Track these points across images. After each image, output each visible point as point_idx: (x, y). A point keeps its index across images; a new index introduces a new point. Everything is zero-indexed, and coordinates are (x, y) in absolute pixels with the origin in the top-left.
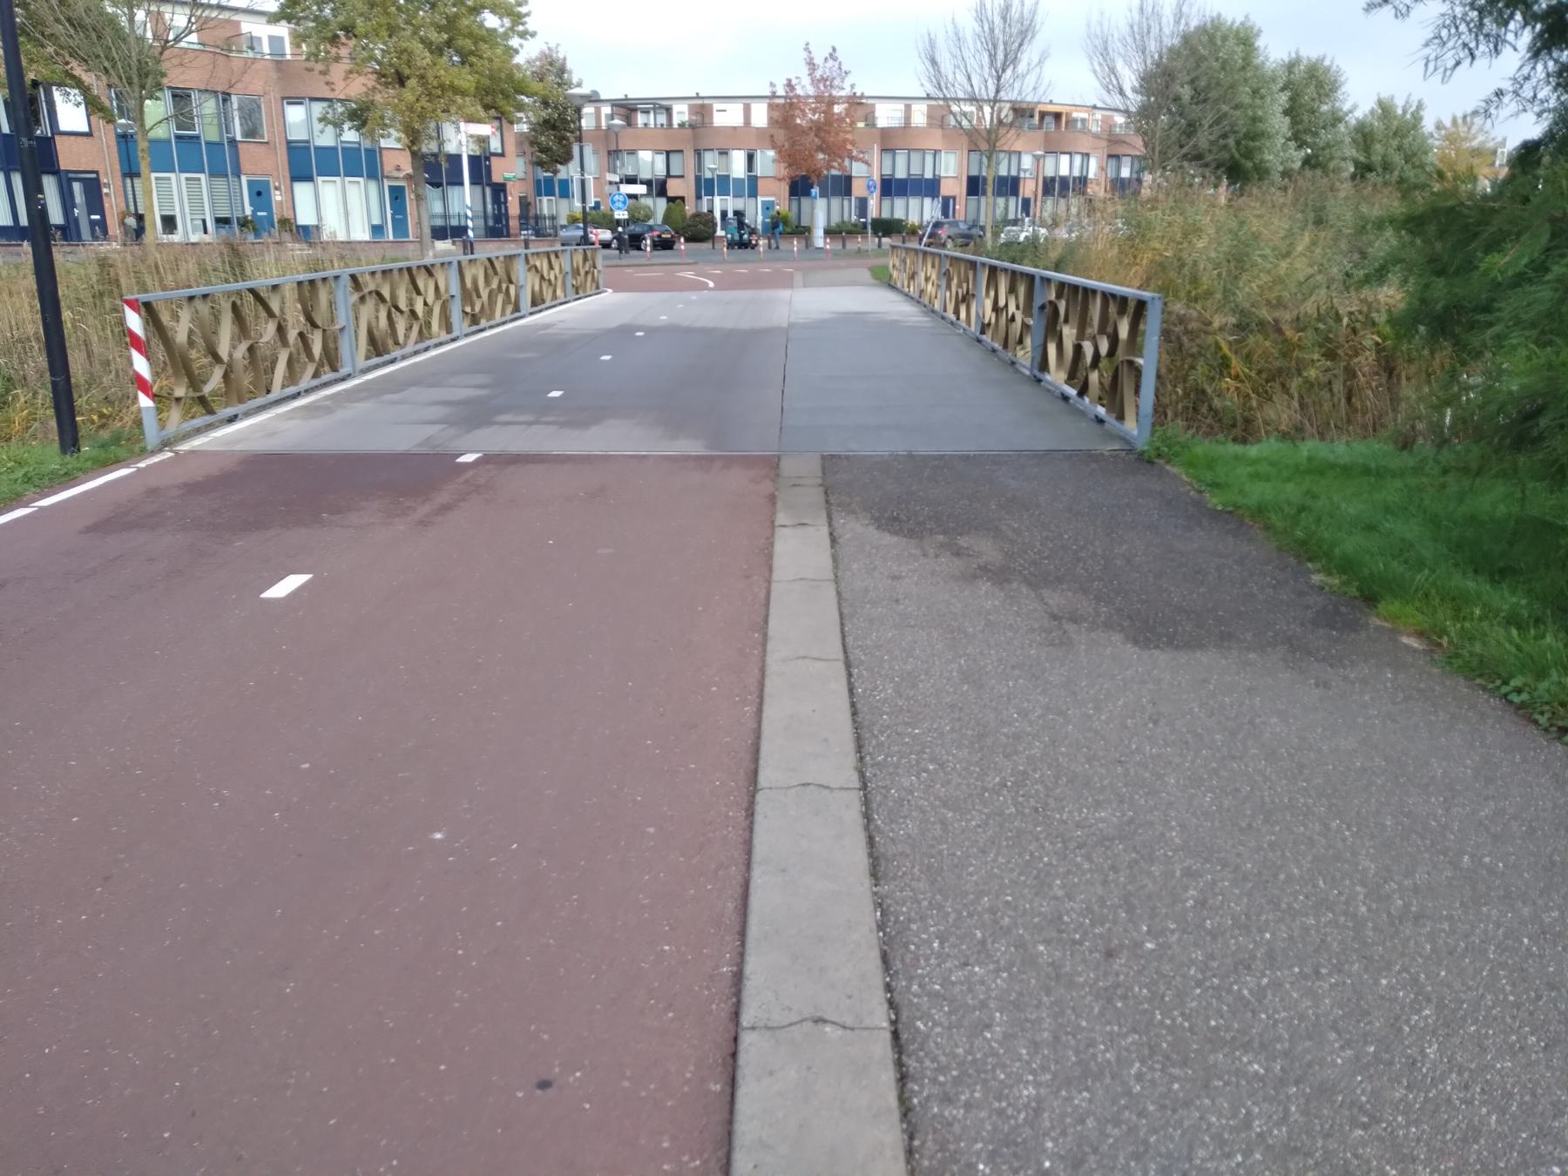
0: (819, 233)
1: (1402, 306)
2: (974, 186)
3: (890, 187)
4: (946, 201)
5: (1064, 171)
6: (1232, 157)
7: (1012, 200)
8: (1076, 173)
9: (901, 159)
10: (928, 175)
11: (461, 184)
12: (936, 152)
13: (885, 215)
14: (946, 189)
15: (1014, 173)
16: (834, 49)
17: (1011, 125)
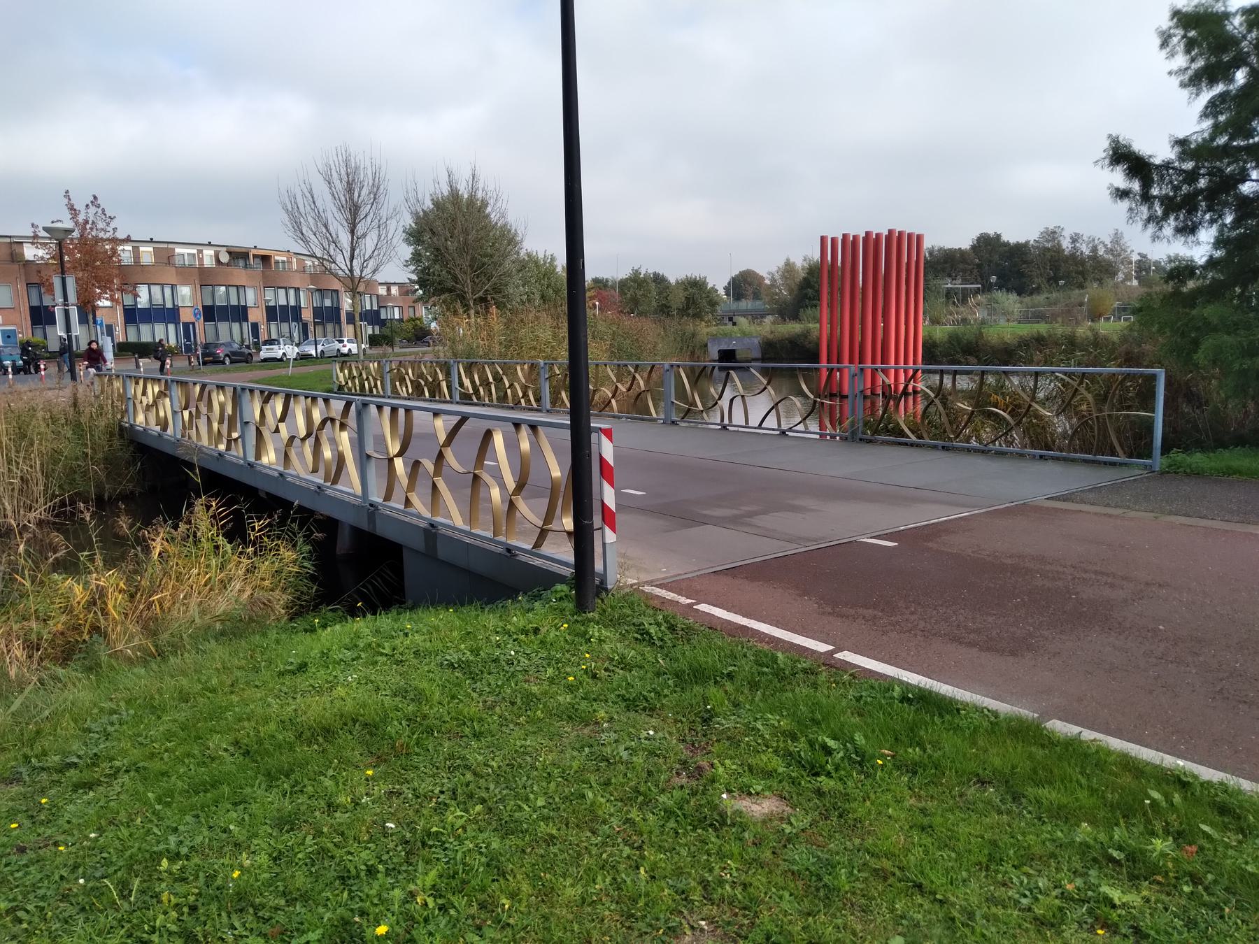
0: (109, 355)
1: (1229, 28)
2: (210, 313)
3: (210, 313)
4: (186, 325)
5: (282, 302)
6: (820, 338)
7: (245, 324)
8: (292, 303)
9: (143, 291)
10: (169, 305)
11: (55, 323)
12: (173, 286)
13: (132, 338)
14: (186, 316)
15: (242, 303)
16: (95, 197)
17: (228, 265)
